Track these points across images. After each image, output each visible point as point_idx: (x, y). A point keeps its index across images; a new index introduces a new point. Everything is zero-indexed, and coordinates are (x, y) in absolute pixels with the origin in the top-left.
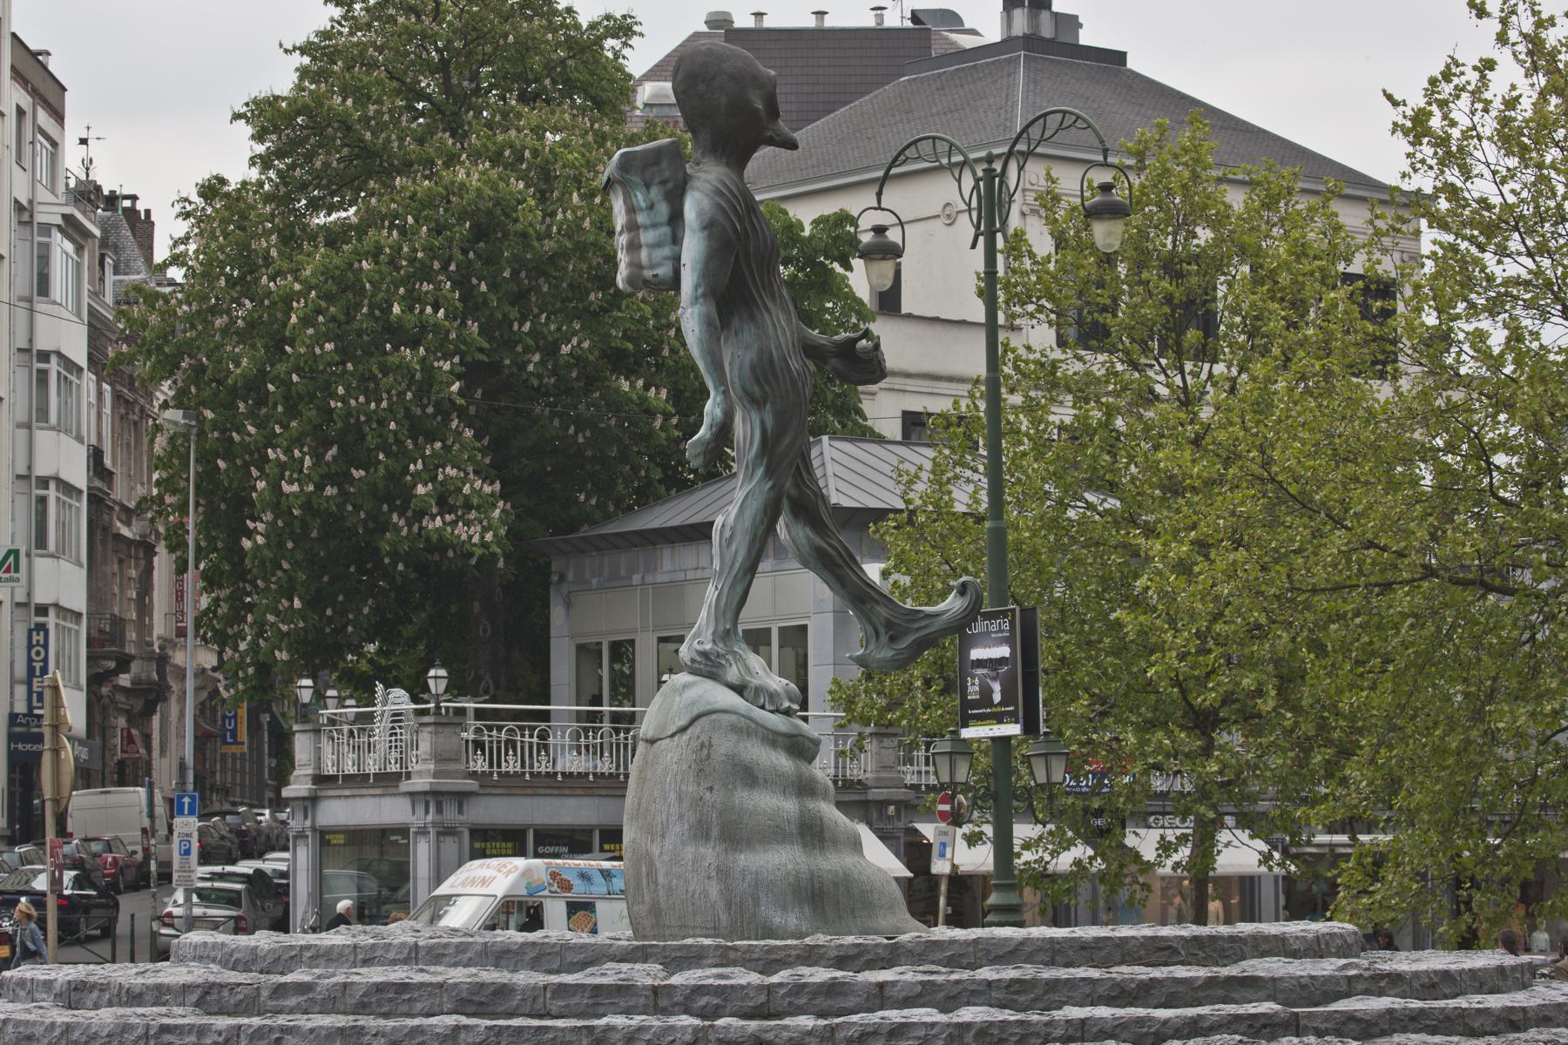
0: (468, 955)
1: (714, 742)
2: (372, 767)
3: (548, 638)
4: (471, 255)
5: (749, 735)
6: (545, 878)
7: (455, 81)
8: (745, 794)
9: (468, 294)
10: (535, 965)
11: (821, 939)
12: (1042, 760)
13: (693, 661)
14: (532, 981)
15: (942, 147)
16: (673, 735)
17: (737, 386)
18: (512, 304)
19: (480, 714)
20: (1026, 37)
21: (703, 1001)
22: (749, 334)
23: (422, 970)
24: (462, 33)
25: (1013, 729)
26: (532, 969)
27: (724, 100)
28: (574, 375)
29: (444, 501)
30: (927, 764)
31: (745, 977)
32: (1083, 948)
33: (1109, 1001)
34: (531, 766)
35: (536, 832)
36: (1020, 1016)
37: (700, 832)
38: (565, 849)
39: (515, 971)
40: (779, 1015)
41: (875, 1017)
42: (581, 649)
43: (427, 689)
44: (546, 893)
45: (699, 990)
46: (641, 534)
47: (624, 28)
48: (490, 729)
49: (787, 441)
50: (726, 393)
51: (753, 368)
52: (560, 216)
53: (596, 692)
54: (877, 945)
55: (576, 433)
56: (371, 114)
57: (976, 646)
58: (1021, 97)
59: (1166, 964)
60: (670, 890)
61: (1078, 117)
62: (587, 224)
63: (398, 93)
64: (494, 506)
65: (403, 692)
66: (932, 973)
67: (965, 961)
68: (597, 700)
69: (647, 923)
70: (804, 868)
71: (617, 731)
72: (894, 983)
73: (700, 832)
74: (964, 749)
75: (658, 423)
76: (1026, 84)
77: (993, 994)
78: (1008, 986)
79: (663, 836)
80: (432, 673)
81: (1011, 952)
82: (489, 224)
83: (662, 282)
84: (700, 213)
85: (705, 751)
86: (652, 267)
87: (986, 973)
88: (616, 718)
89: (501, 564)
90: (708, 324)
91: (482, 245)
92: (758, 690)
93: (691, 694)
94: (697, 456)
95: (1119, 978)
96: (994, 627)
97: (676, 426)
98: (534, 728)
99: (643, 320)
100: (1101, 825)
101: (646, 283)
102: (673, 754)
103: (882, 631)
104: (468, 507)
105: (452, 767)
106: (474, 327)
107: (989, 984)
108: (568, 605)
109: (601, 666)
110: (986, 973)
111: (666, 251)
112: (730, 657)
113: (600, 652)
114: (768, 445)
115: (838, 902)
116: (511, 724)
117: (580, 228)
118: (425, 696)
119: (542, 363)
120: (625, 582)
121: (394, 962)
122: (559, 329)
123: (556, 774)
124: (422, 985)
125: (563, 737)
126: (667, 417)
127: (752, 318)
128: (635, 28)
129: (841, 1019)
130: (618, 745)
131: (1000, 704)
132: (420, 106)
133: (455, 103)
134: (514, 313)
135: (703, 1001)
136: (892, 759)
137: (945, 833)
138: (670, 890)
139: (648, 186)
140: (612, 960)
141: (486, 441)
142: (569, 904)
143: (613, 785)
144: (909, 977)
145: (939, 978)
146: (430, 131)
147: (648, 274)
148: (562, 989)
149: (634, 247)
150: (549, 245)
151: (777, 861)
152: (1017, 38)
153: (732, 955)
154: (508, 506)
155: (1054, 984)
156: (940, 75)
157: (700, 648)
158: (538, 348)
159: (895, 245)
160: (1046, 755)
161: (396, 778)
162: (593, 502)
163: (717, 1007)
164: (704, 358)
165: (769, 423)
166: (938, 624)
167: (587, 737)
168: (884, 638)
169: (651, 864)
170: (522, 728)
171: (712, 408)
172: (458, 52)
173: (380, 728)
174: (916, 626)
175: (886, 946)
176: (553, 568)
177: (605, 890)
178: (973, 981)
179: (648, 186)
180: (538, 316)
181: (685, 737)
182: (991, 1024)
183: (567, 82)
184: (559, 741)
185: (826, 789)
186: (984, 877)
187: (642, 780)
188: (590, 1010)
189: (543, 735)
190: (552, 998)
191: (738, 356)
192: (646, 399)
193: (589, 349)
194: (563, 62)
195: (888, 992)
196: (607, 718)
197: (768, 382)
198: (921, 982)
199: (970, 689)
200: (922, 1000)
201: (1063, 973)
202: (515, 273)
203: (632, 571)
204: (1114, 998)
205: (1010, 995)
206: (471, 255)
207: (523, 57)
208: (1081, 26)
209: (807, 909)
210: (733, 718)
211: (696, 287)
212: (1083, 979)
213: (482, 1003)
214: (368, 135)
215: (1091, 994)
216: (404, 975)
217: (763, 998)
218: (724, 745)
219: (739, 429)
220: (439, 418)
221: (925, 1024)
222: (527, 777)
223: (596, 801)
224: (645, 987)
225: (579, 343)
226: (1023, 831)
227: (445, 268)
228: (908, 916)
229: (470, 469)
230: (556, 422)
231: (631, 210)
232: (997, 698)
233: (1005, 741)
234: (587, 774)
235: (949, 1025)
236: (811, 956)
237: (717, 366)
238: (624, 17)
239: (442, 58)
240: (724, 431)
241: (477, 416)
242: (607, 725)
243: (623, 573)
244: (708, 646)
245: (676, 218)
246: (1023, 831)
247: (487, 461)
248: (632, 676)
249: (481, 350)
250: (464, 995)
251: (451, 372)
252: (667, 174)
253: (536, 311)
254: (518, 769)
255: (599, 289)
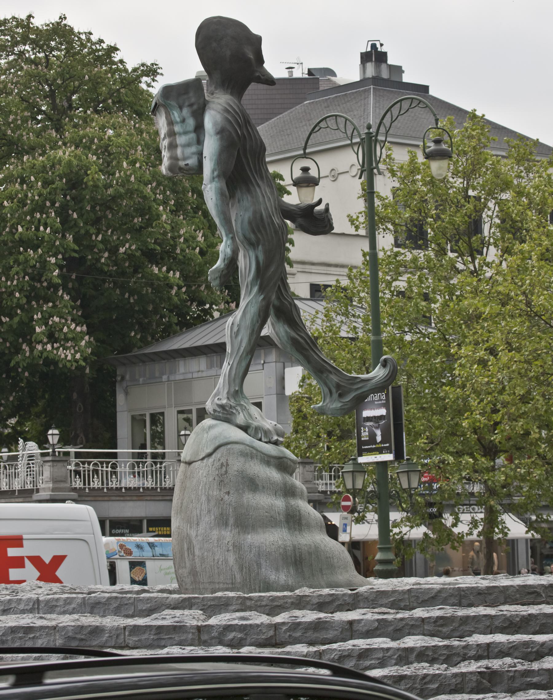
0: (73, 606)
1: (230, 462)
2: (17, 485)
3: (116, 412)
4: (68, 198)
5: (252, 458)
6: (117, 548)
7: (58, 101)
8: (250, 496)
9: (65, 220)
10: (117, 612)
11: (306, 591)
12: (406, 474)
13: (215, 411)
14: (116, 624)
15: (341, 121)
16: (203, 459)
17: (240, 234)
18: (92, 225)
19: (78, 455)
20: (373, 78)
21: (231, 636)
22: (247, 201)
23: (41, 618)
24: (61, 75)
25: (389, 457)
26: (115, 615)
27: (228, 53)
28: (127, 264)
29: (52, 337)
30: (330, 479)
31: (262, 619)
32: (479, 594)
33: (503, 630)
34: (107, 484)
35: (110, 521)
36: (446, 642)
37: (222, 521)
38: (127, 531)
39: (104, 616)
40: (282, 644)
41: (349, 644)
42: (133, 418)
43: (47, 441)
44: (117, 556)
45: (228, 628)
46: (166, 352)
47: (152, 71)
48: (83, 463)
49: (272, 269)
50: (233, 239)
51: (250, 223)
52: (117, 175)
53: (143, 442)
54: (344, 595)
55: (129, 297)
56: (10, 120)
57: (366, 409)
58: (370, 111)
59: (534, 604)
60: (203, 559)
61: (420, 101)
62: (132, 179)
63: (26, 109)
64: (82, 339)
65: (34, 444)
66: (384, 613)
67: (402, 604)
68: (144, 446)
69: (188, 580)
70: (289, 543)
71: (156, 463)
72: (359, 621)
73: (222, 521)
74: (360, 469)
75: (174, 292)
76: (375, 103)
77: (426, 627)
78: (435, 622)
79: (198, 524)
80: (50, 432)
81: (433, 597)
82: (75, 181)
83: (191, 169)
84: (215, 124)
85: (224, 469)
86: (184, 159)
87: (419, 613)
88: (154, 456)
89: (87, 371)
90: (221, 194)
91: (74, 191)
92: (257, 429)
93: (214, 432)
94: (215, 279)
95: (508, 614)
96: (376, 398)
97: (185, 293)
98: (109, 462)
99: (165, 234)
100: (429, 512)
101: (181, 169)
102: (203, 471)
103: (334, 390)
104: (67, 340)
105: (62, 485)
106: (70, 238)
107: (423, 620)
108: (127, 393)
109: (145, 427)
110: (419, 613)
111: (194, 149)
112: (239, 408)
113: (145, 421)
114: (261, 272)
115: (311, 565)
116: (95, 461)
117: (128, 181)
118: (47, 446)
119: (109, 258)
120: (158, 380)
121: (23, 612)
122: (118, 239)
123: (121, 488)
124: (42, 628)
125: (125, 467)
126: (180, 287)
127: (249, 191)
128: (159, 71)
129: (326, 647)
130: (156, 472)
131: (381, 442)
132: (39, 117)
133: (58, 114)
134: (93, 230)
135: (231, 636)
136: (311, 476)
137: (346, 518)
138: (203, 559)
139: (181, 108)
140: (168, 608)
141: (79, 303)
142: (130, 562)
143: (167, 494)
144: (369, 616)
145: (390, 617)
146: (45, 128)
147: (182, 164)
148: (136, 629)
149: (172, 146)
150: (110, 191)
151: (272, 539)
152: (369, 78)
153: (248, 603)
154: (92, 339)
155: (465, 620)
156: (326, 100)
157: (219, 402)
158: (106, 249)
159: (314, 178)
160: (407, 472)
161: (31, 492)
162: (139, 337)
163: (241, 639)
164: (219, 217)
165: (261, 258)
166: (369, 385)
167: (139, 467)
168: (335, 395)
169: (190, 542)
170: (102, 463)
171: (224, 248)
172: (59, 86)
173: (21, 465)
174: (355, 387)
175: (350, 595)
176: (118, 373)
177: (151, 554)
178: (412, 619)
179: (181, 108)
180: (106, 231)
181: (211, 460)
182: (427, 648)
183: (119, 102)
184: (123, 469)
185: (302, 492)
186: (374, 542)
187: (184, 489)
188: (156, 643)
189: (114, 466)
190: (130, 635)
191: (241, 215)
192: (168, 277)
193: (135, 250)
194: (118, 90)
195: (355, 627)
196: (149, 456)
197: (260, 231)
198: (378, 620)
199: (363, 434)
200: (378, 632)
201: (472, 611)
202: (93, 208)
203: (163, 374)
204: (505, 628)
205: (437, 627)
206: (68, 198)
207: (96, 88)
208: (403, 72)
209: (292, 571)
210: (241, 447)
211: (213, 172)
212: (485, 616)
213: (82, 640)
214: (9, 132)
215: (491, 625)
216: (29, 621)
217: (271, 633)
218: (236, 464)
219: (242, 262)
220: (52, 290)
221: (382, 649)
222: (105, 490)
223: (144, 503)
224: (192, 627)
225: (130, 247)
226: (395, 516)
227: (53, 203)
228: (356, 573)
229: (70, 318)
230: (118, 291)
231: (170, 123)
232: (379, 439)
233: (384, 465)
234: (139, 488)
235: (398, 649)
236: (301, 603)
237: (227, 221)
238: (152, 64)
239: (51, 90)
240: (232, 263)
241: (73, 288)
242: (149, 460)
243: (157, 374)
244: (224, 401)
245: (199, 128)
246: (395, 516)
247: (80, 313)
248: (163, 432)
249: (75, 251)
250: (70, 634)
251: (56, 264)
252: (193, 100)
253: (104, 228)
254: (100, 486)
255: (141, 216)
